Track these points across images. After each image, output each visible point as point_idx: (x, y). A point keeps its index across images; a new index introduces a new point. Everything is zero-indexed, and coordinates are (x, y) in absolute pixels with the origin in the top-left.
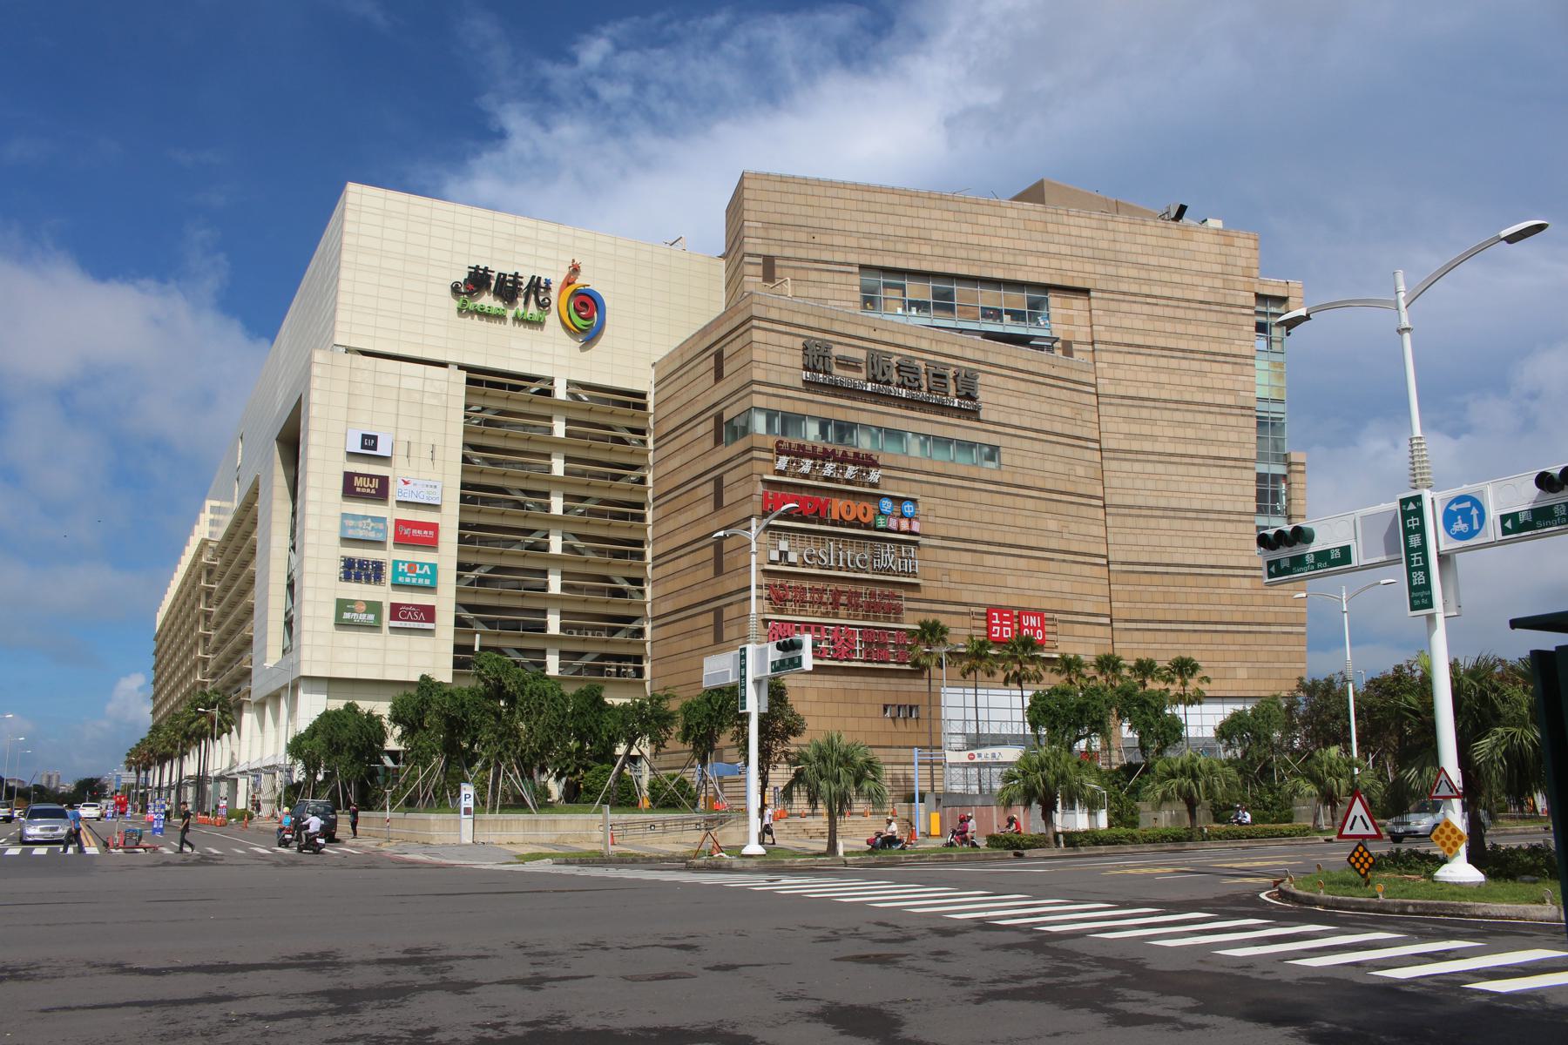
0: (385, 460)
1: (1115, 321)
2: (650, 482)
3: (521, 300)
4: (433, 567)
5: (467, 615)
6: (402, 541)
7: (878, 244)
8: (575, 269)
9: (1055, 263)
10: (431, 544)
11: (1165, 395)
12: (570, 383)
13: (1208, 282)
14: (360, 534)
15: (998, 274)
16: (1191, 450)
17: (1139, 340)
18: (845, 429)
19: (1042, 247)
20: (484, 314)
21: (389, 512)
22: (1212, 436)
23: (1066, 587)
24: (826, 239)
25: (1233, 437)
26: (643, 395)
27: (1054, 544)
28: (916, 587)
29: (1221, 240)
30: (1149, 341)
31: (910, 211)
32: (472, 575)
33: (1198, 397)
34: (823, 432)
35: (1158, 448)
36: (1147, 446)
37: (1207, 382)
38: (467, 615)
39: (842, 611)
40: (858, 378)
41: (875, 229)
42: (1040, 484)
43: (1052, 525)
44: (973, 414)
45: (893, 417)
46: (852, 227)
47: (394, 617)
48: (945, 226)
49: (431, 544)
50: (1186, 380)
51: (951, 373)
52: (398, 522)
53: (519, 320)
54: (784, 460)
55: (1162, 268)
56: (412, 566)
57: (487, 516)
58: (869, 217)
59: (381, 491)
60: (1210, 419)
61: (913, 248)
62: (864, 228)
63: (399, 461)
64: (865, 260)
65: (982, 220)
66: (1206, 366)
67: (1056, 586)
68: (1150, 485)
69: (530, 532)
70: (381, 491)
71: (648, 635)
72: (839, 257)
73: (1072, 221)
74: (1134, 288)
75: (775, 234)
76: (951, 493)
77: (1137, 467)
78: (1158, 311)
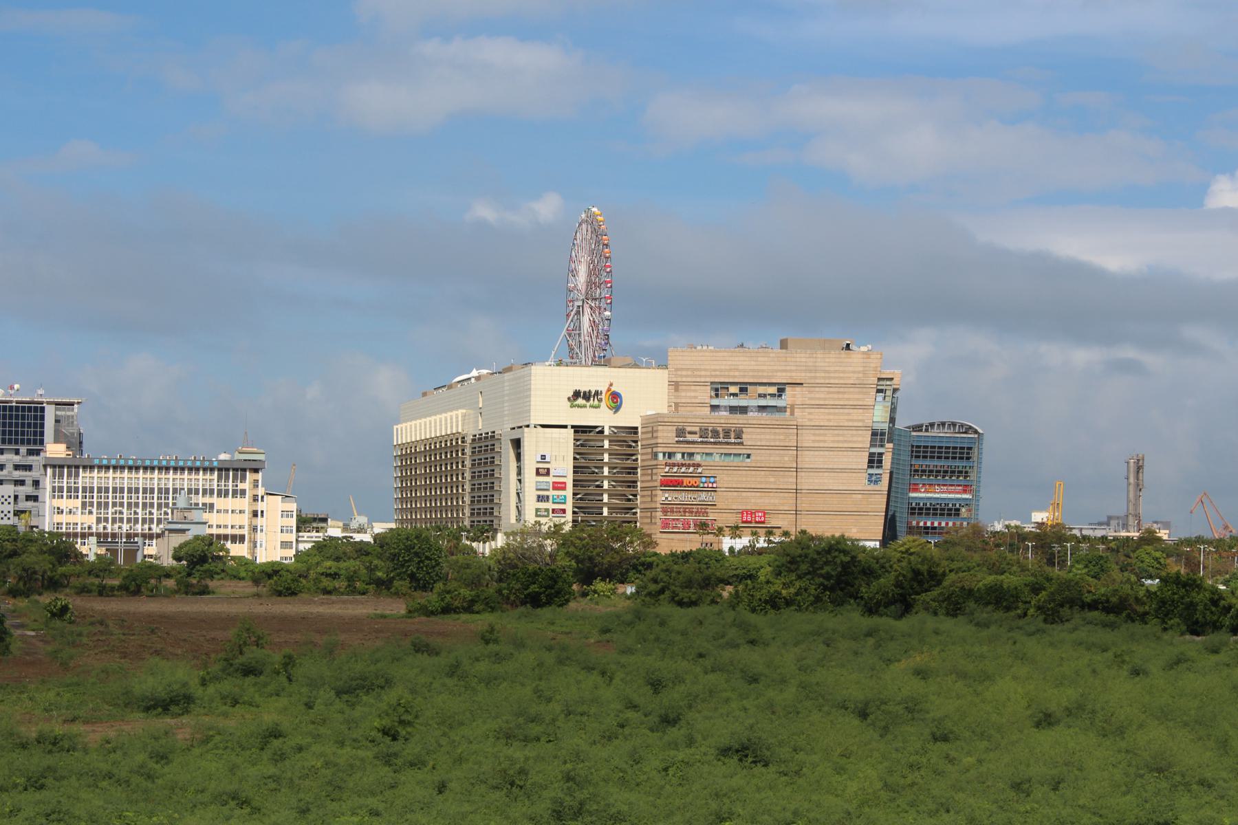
0: (548, 462)
1: (812, 395)
2: (639, 461)
3: (592, 399)
4: (565, 496)
5: (576, 510)
6: (555, 488)
7: (718, 373)
8: (611, 385)
9: (789, 374)
10: (564, 489)
11: (831, 424)
12: (610, 427)
13: (856, 375)
14: (542, 487)
15: (765, 381)
16: (841, 445)
17: (822, 402)
18: (691, 455)
19: (783, 368)
20: (579, 406)
21: (550, 479)
22: (851, 439)
23: (777, 501)
24: (698, 373)
25: (860, 439)
26: (637, 428)
27: (772, 486)
28: (715, 505)
29: (865, 356)
30: (827, 403)
31: (731, 359)
32: (578, 443)
33: (846, 424)
34: (683, 456)
35: (826, 445)
36: (822, 445)
37: (850, 417)
38: (576, 510)
39: (687, 514)
40: (696, 438)
41: (717, 367)
42: (768, 465)
43: (772, 480)
44: (741, 444)
45: (708, 449)
46: (708, 367)
47: (553, 513)
48: (745, 363)
49: (564, 489)
50: (842, 417)
51: (733, 429)
52: (553, 483)
53: (591, 406)
54: (668, 468)
55: (836, 371)
56: (558, 496)
57: (581, 477)
58: (715, 363)
59: (548, 473)
60: (850, 432)
61: (732, 374)
62: (713, 367)
63: (553, 462)
64: (713, 380)
65: (760, 359)
66: (851, 411)
67: (772, 501)
68: (821, 460)
69: (597, 481)
70: (548, 473)
71: (638, 515)
72: (703, 380)
73: (798, 355)
74: (822, 381)
75: (679, 373)
76: (730, 472)
77: (817, 453)
78: (831, 389)
